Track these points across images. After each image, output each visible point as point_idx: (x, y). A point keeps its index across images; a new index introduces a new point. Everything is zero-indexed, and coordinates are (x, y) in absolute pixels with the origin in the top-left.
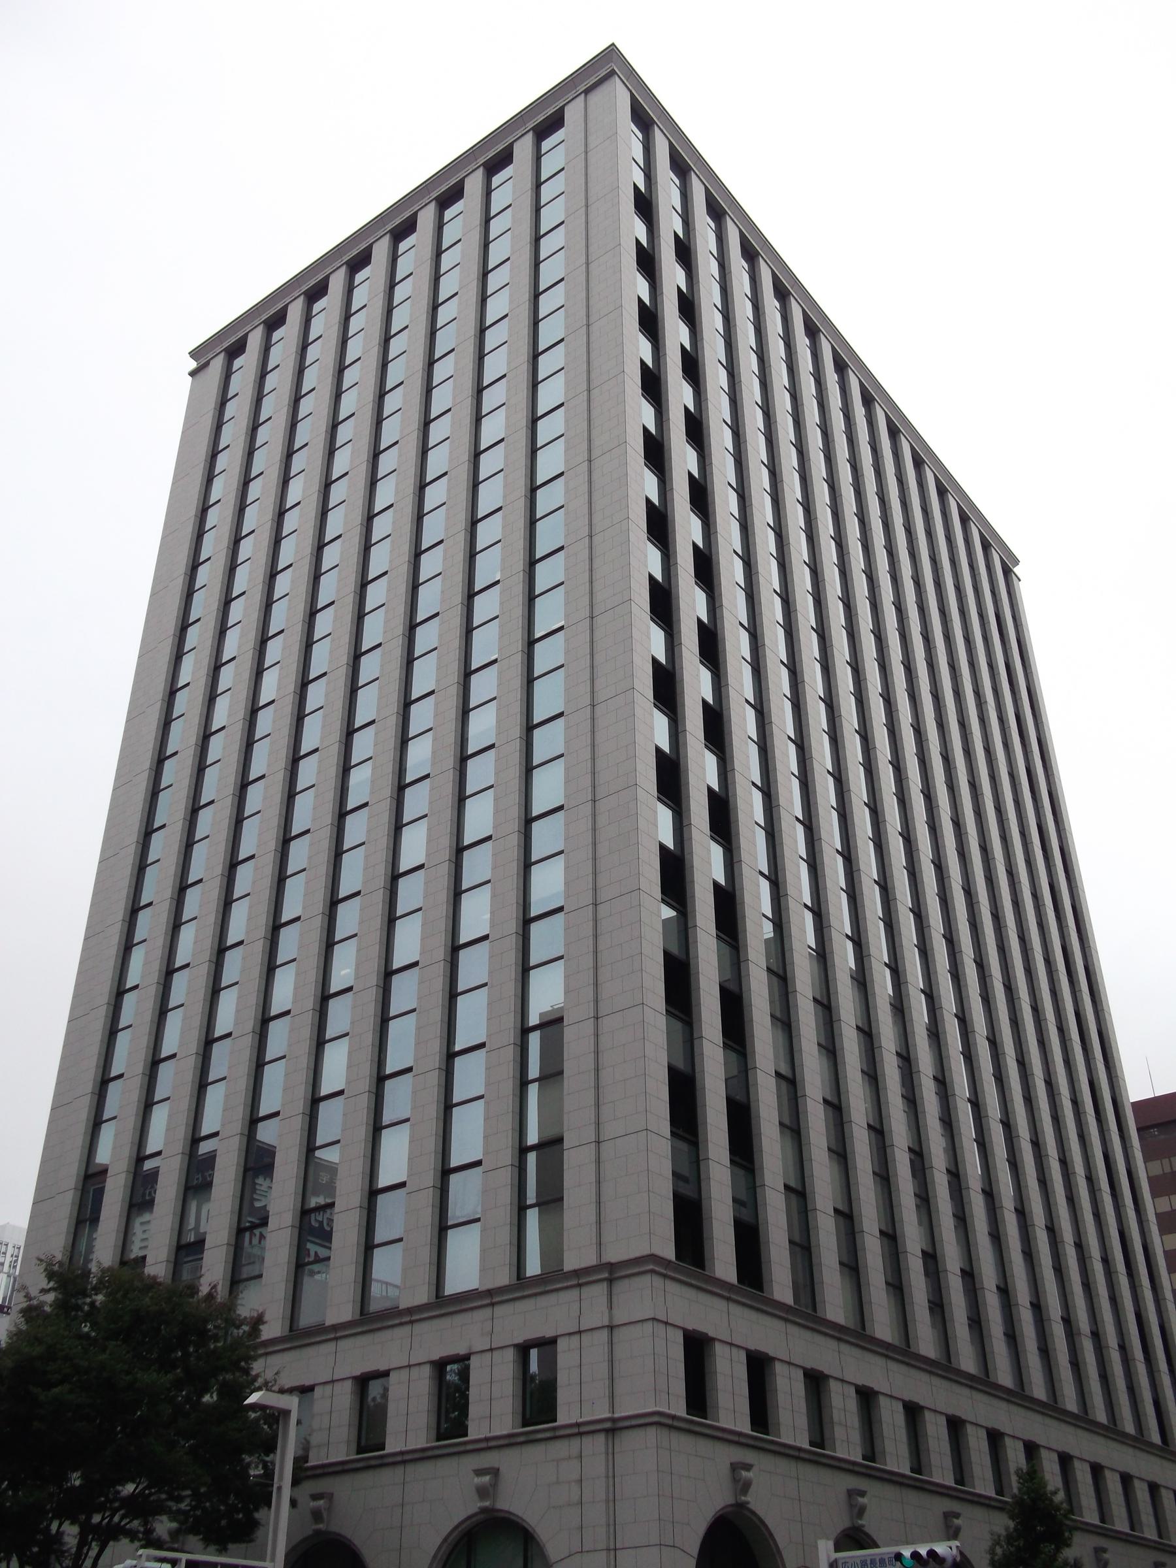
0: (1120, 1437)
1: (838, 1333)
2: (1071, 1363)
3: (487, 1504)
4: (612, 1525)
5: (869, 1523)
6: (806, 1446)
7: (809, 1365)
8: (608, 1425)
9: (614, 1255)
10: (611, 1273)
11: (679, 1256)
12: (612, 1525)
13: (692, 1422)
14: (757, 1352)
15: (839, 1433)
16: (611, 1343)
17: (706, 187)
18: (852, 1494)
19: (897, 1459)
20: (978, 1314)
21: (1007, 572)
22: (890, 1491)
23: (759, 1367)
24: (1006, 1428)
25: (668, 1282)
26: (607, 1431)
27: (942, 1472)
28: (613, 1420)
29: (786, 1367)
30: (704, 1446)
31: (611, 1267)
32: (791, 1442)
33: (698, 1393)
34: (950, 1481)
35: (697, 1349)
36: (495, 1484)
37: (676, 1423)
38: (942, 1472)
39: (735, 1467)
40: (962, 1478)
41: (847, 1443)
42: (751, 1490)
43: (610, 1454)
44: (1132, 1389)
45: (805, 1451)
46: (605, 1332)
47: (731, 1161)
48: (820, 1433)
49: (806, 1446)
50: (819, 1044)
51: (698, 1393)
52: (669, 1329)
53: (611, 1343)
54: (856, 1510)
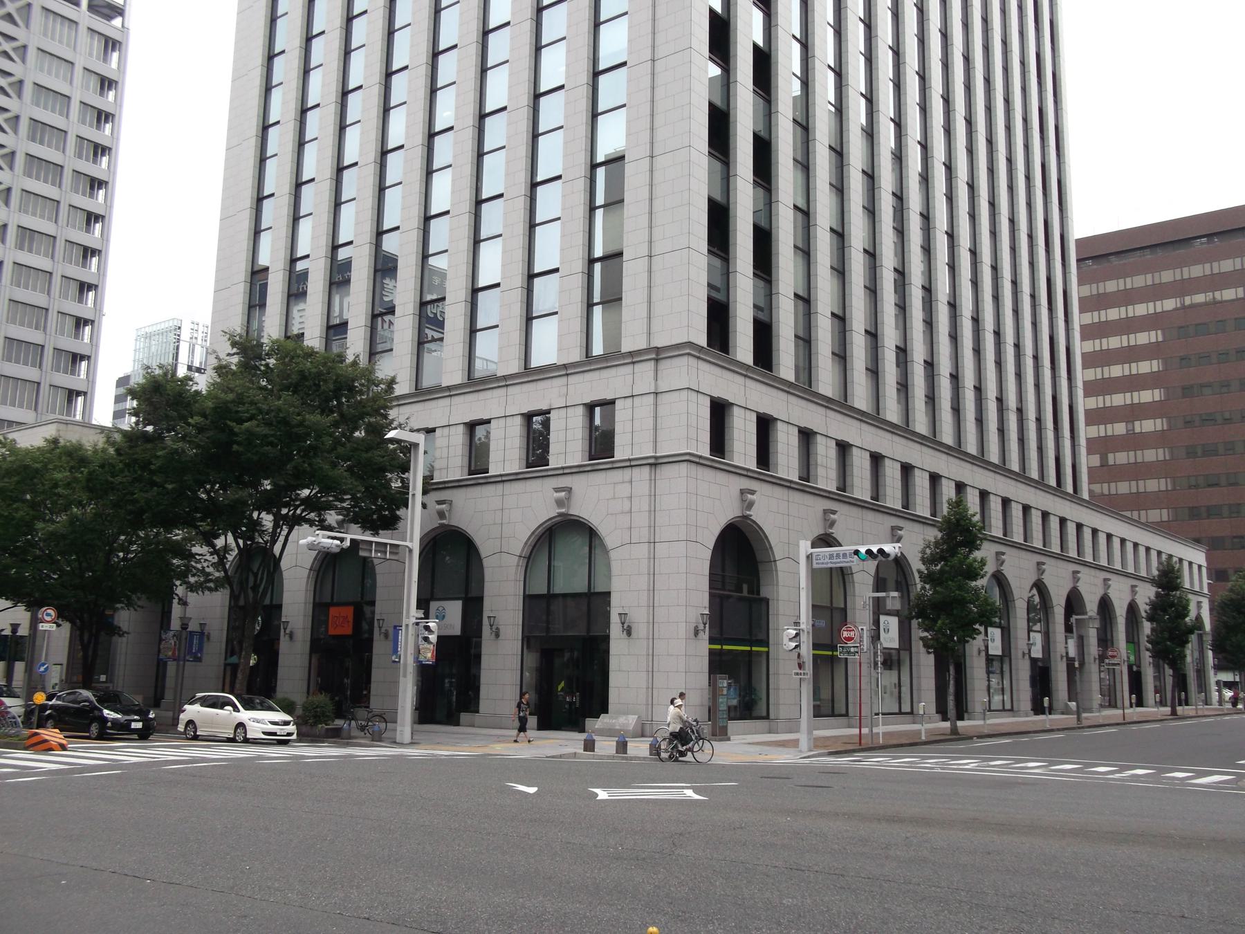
5: (837, 532)
9: (659, 342)
23: (765, 425)
30: (722, 477)
33: (719, 442)
35: (720, 411)
36: (569, 499)
43: (653, 481)
51: (719, 442)
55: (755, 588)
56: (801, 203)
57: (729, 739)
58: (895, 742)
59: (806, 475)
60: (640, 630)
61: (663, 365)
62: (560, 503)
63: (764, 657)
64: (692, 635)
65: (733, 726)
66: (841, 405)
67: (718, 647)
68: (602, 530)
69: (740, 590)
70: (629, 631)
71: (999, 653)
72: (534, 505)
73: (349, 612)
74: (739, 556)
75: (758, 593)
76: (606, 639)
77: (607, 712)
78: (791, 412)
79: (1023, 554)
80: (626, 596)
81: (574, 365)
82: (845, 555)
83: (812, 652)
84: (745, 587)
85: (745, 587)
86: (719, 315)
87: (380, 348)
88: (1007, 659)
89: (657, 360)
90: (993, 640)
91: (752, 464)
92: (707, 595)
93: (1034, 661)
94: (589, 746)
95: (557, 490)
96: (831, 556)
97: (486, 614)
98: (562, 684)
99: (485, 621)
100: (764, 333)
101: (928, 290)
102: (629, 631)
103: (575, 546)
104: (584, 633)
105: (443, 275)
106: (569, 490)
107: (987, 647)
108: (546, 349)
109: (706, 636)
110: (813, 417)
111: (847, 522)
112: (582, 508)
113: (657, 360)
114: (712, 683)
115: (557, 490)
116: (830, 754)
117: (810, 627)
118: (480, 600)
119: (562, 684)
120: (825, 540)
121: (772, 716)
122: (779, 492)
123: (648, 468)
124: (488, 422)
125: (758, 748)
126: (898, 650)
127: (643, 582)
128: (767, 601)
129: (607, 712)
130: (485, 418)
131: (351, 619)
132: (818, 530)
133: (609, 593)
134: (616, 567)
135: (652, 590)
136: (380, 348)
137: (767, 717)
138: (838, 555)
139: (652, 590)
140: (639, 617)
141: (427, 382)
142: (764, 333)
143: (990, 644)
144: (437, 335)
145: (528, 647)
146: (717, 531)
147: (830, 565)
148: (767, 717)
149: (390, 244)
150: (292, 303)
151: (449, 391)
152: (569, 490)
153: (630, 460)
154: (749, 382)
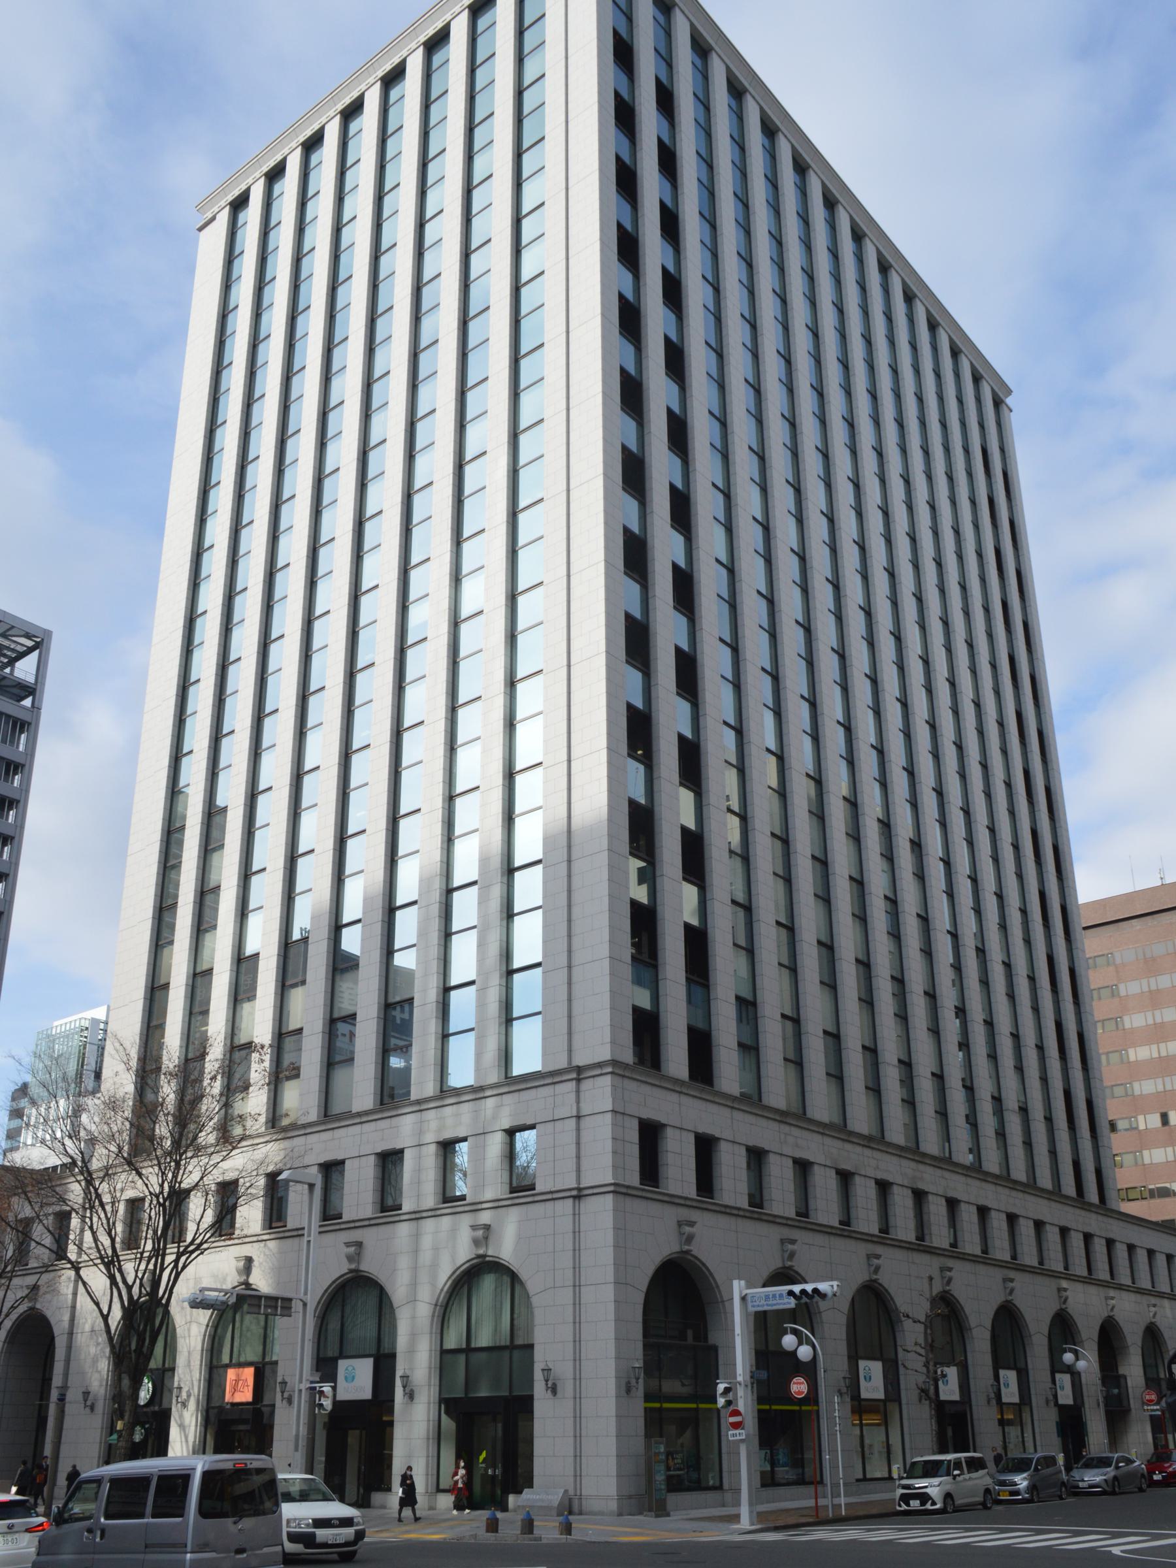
0: (1014, 1185)
1: (782, 1117)
2: (1049, 1151)
3: (481, 1252)
4: (576, 1268)
5: (799, 1265)
6: (746, 1206)
7: (751, 1143)
8: (574, 1193)
9: (580, 1060)
10: (579, 1074)
11: (691, 1077)
12: (576, 1268)
13: (643, 1190)
14: (649, 1120)
15: (935, 1229)
16: (578, 1130)
17: (851, 217)
18: (1007, 1280)
19: (971, 1245)
20: (879, 1085)
21: (998, 403)
22: (968, 1266)
23: (705, 1146)
24: (1046, 1218)
25: (626, 1081)
26: (574, 1197)
27: (1001, 1251)
28: (579, 1189)
29: (778, 1157)
30: (655, 1208)
31: (579, 1069)
32: (866, 1230)
33: (650, 1169)
34: (978, 1252)
35: (650, 1135)
36: (486, 1238)
37: (630, 1192)
38: (1001, 1251)
39: (869, 1257)
40: (923, 1234)
41: (867, 1219)
42: (694, 1242)
43: (576, 1215)
44: (1053, 1153)
45: (744, 1210)
46: (574, 1120)
47: (687, 979)
48: (757, 1199)
49: (746, 1206)
50: (853, 915)
51: (650, 1169)
52: (626, 1118)
53: (578, 1130)
54: (872, 1269)
55: (702, 1333)
56: (741, 897)
57: (668, 1515)
58: (861, 1513)
59: (757, 1199)
60: (567, 1389)
61: (586, 1085)
62: (350, 1258)
63: (815, 1417)
64: (623, 1393)
65: (673, 1499)
66: (796, 1116)
67: (767, 1407)
68: (523, 1274)
69: (683, 1337)
70: (554, 1390)
71: (1016, 1400)
72: (446, 1246)
73: (249, 1373)
74: (676, 1302)
75: (706, 1339)
76: (531, 1398)
77: (531, 1486)
78: (736, 1131)
79: (1039, 1280)
80: (550, 1349)
81: (310, 1125)
82: (781, 1296)
83: (757, 1407)
84: (690, 1333)
85: (690, 1333)
86: (646, 1027)
87: (338, 1058)
88: (1026, 1410)
89: (578, 1080)
90: (1062, 1388)
91: (691, 1191)
92: (640, 1345)
93: (1062, 1409)
94: (493, 1525)
95: (348, 1245)
96: (767, 1297)
97: (399, 1373)
98: (484, 1455)
99: (538, 1376)
100: (701, 1044)
101: (899, 981)
102: (554, 1390)
103: (366, 1302)
104: (506, 1393)
105: (409, 974)
106: (359, 1245)
107: (1055, 1396)
108: (462, 1074)
109: (640, 1392)
110: (765, 1134)
111: (810, 1250)
112: (506, 1249)
113: (578, 1080)
114: (648, 1447)
115: (348, 1245)
116: (776, 1529)
117: (748, 1377)
118: (392, 1356)
119: (484, 1455)
120: (783, 1276)
121: (726, 1486)
122: (723, 1221)
123: (571, 1200)
124: (342, 1162)
125: (695, 1525)
126: (884, 1401)
127: (567, 1332)
128: (715, 1349)
129: (531, 1486)
130: (339, 1158)
131: (251, 1382)
132: (775, 1263)
133: (531, 1347)
134: (539, 1316)
135: (577, 1341)
136: (338, 1058)
137: (719, 1487)
138: (774, 1296)
139: (577, 1341)
140: (563, 1370)
141: (337, 1108)
142: (701, 1044)
143: (1059, 1392)
144: (401, 1043)
145: (447, 1413)
146: (650, 1270)
147: (766, 1308)
148: (719, 1487)
149: (351, 941)
150: (338, 978)
151: (361, 1117)
152: (359, 1245)
153: (551, 1192)
154: (684, 1099)
